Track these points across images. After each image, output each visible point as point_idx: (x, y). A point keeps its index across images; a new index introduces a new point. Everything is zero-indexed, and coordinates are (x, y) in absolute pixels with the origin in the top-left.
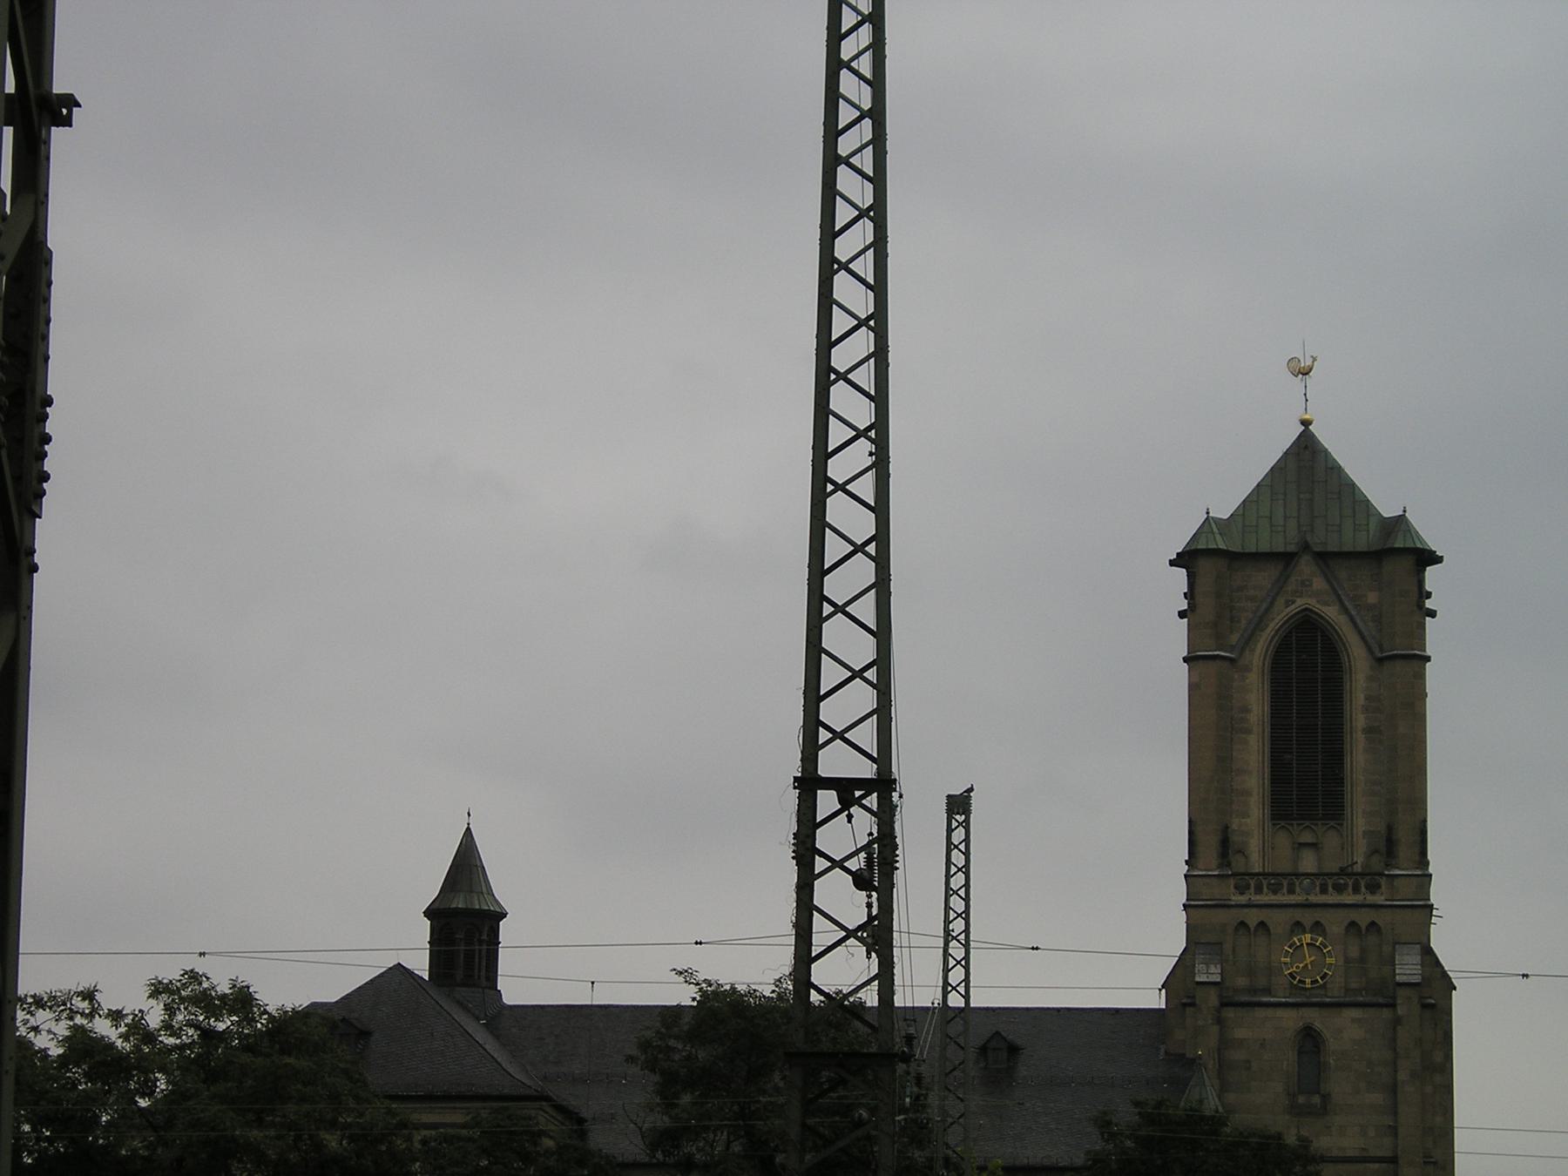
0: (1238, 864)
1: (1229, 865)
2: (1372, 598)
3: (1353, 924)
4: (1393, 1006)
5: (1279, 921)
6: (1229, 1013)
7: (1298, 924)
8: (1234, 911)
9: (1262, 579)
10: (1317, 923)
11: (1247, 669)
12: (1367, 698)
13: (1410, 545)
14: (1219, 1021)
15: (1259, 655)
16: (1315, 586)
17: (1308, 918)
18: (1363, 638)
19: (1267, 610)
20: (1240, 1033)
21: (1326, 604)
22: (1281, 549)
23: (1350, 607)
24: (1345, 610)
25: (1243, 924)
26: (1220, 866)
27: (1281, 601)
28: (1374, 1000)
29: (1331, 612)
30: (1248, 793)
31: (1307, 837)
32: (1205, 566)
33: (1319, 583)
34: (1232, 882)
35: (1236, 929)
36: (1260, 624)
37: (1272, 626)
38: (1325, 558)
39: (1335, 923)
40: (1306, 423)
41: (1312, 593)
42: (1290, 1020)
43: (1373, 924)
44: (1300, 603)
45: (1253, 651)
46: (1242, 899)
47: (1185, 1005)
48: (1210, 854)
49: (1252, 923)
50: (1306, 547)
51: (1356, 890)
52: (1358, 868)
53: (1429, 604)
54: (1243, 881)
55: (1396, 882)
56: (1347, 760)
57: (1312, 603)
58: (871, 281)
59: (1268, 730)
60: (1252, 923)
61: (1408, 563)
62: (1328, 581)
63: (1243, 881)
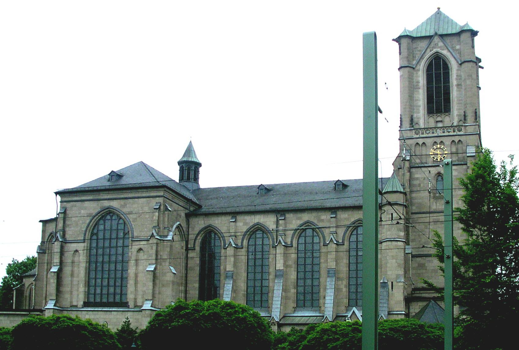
0: (416, 127)
1: (413, 127)
2: (458, 47)
3: (453, 141)
4: (466, 164)
5: (429, 142)
6: (413, 170)
7: (435, 142)
8: (414, 140)
9: (423, 44)
10: (442, 142)
11: (419, 70)
12: (457, 76)
13: (468, 29)
14: (409, 171)
15: (422, 67)
16: (439, 45)
17: (438, 140)
18: (454, 58)
19: (424, 53)
20: (417, 176)
21: (443, 50)
22: (428, 35)
23: (451, 51)
24: (449, 51)
25: (417, 143)
26: (410, 127)
27: (429, 50)
28: (460, 163)
29: (445, 52)
30: (420, 106)
31: (439, 119)
32: (404, 41)
33: (441, 44)
34: (414, 131)
35: (415, 146)
36: (422, 58)
37: (425, 59)
38: (442, 36)
39: (447, 141)
40: (439, 9)
41: (439, 47)
42: (434, 171)
43: (460, 141)
44: (435, 50)
45: (420, 65)
46: (418, 136)
47: (399, 169)
48: (407, 125)
49: (421, 143)
50: (436, 34)
51: (454, 131)
52: (455, 124)
53: (480, 64)
54: (417, 130)
55: (467, 127)
56: (451, 95)
57: (439, 50)
58: (425, 303)
59: (426, 88)
60: (421, 143)
61: (468, 34)
62: (444, 43)
63: (417, 130)
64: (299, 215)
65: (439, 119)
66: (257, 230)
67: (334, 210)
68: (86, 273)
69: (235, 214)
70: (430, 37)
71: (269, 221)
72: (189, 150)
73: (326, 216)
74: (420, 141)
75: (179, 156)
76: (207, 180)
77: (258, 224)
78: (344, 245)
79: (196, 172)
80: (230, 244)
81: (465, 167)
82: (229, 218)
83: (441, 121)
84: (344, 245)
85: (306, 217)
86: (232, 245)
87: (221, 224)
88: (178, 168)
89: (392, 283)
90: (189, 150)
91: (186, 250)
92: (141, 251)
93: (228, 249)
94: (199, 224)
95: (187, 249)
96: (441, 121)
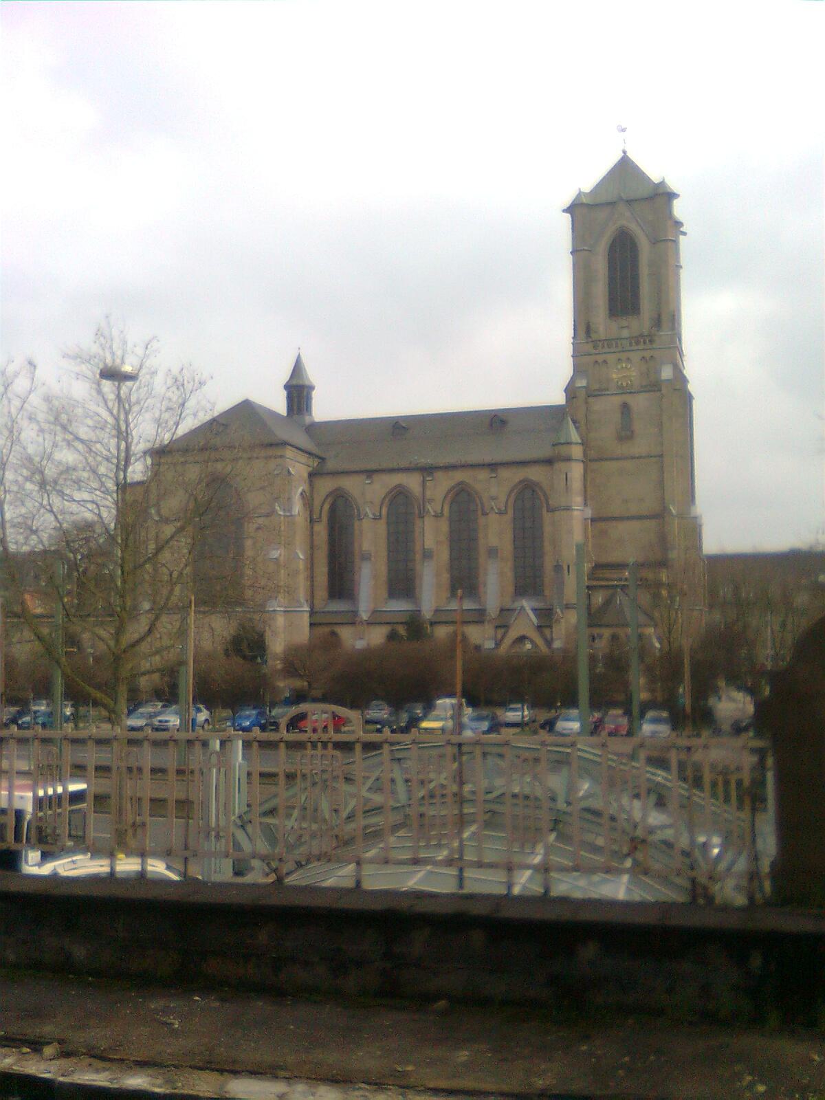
6: (591, 400)
25: (596, 362)
38: (629, 202)
52: (646, 334)
64: (451, 474)
65: (625, 323)
66: (399, 496)
67: (493, 466)
68: (372, 815)
69: (370, 473)
70: (612, 204)
71: (412, 482)
72: (298, 369)
73: (483, 475)
74: (600, 358)
75: (285, 376)
76: (324, 409)
77: (399, 486)
78: (506, 513)
79: (308, 399)
80: (366, 515)
81: (658, 394)
82: (363, 477)
83: (627, 327)
84: (506, 513)
85: (459, 476)
86: (368, 515)
87: (351, 485)
88: (284, 393)
89: (569, 567)
90: (298, 369)
91: (310, 522)
92: (260, 531)
93: (364, 520)
94: (325, 486)
95: (312, 521)
96: (627, 327)
